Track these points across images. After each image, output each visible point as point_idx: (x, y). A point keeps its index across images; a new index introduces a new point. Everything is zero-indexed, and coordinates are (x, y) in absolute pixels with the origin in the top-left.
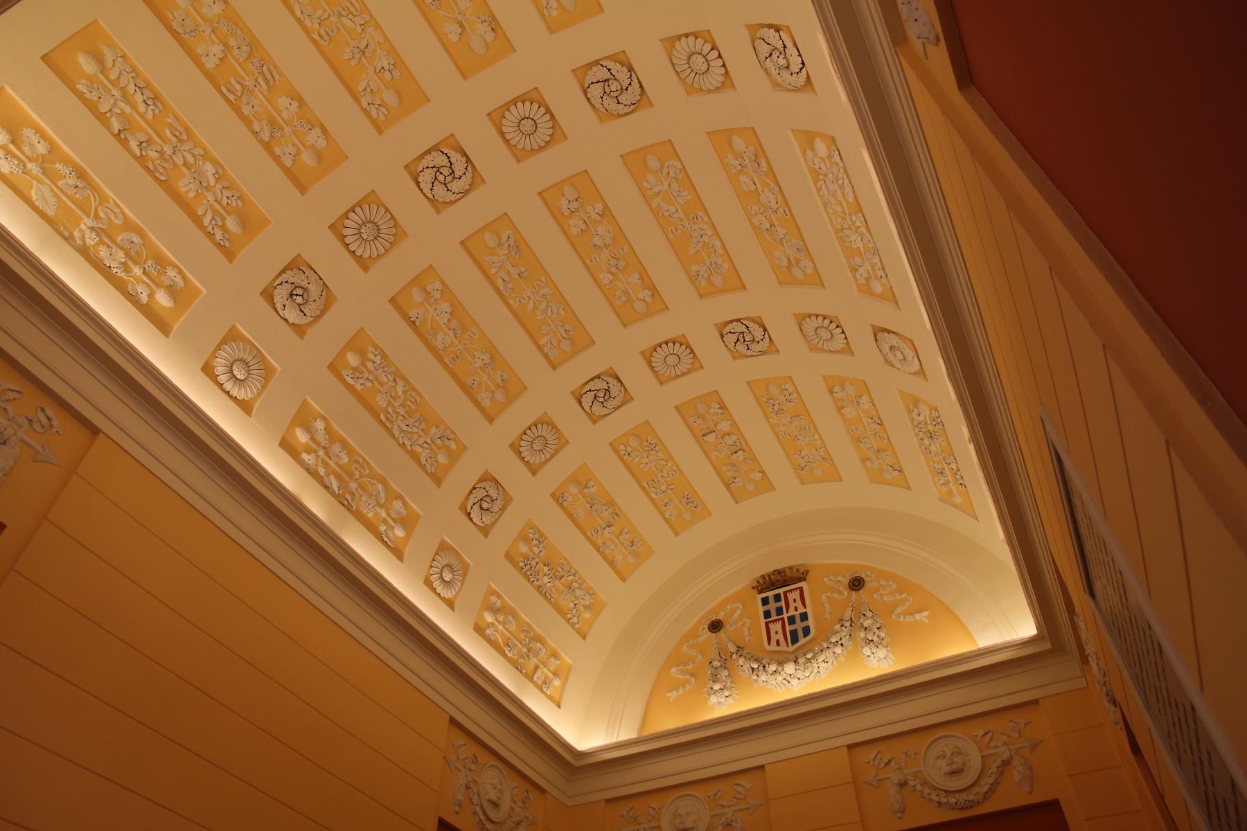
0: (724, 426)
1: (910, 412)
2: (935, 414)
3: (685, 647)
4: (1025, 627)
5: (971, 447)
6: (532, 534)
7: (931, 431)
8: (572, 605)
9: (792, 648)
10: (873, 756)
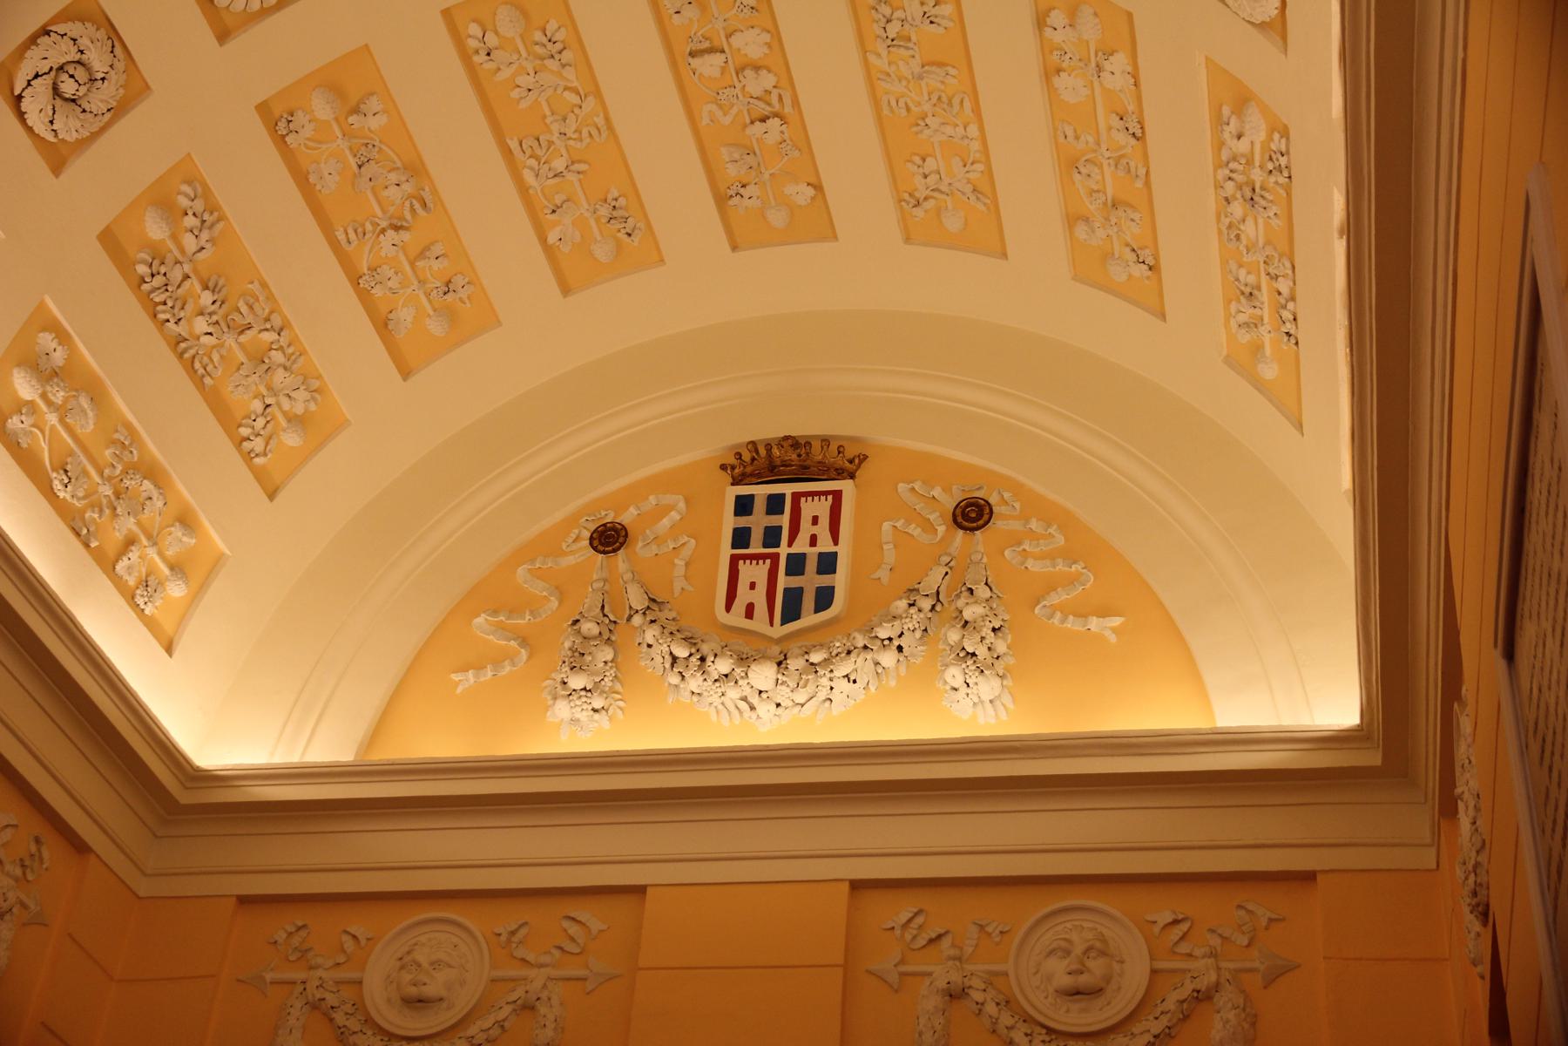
0: (751, 44)
1: (1219, 122)
2: (1278, 143)
3: (521, 571)
4: (1336, 703)
5: (1340, 247)
6: (185, 196)
7: (1256, 186)
8: (257, 406)
9: (779, 630)
10: (904, 916)
